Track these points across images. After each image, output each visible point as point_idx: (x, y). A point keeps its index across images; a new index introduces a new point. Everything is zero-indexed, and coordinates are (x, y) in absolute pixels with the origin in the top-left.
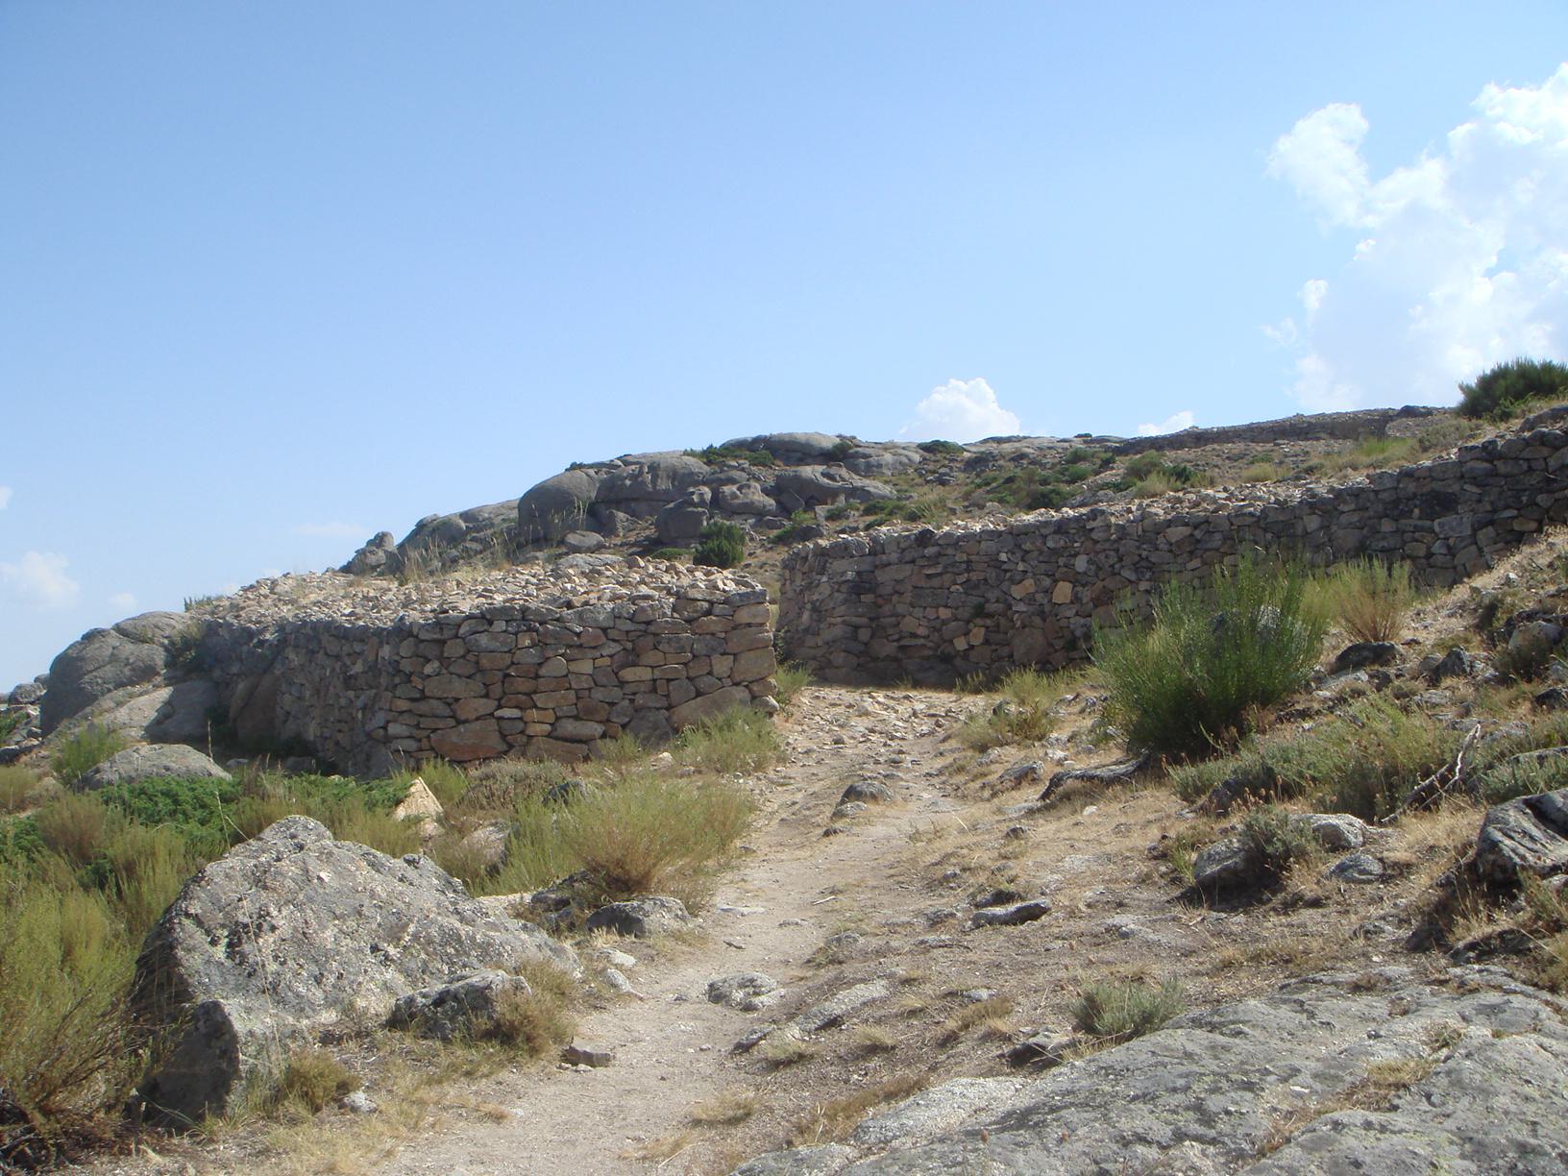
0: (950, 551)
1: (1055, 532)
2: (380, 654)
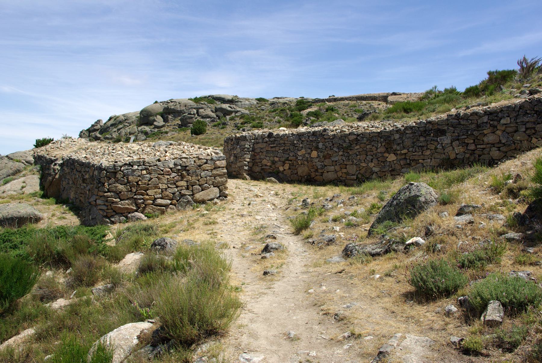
0: (278, 140)
1: (312, 135)
2: (94, 173)
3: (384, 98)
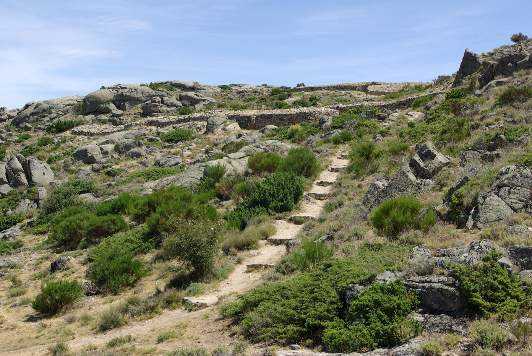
3: (364, 88)
